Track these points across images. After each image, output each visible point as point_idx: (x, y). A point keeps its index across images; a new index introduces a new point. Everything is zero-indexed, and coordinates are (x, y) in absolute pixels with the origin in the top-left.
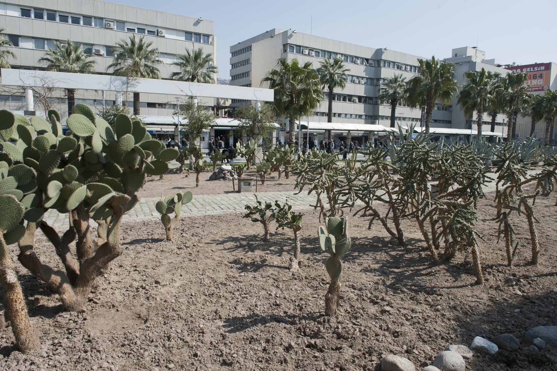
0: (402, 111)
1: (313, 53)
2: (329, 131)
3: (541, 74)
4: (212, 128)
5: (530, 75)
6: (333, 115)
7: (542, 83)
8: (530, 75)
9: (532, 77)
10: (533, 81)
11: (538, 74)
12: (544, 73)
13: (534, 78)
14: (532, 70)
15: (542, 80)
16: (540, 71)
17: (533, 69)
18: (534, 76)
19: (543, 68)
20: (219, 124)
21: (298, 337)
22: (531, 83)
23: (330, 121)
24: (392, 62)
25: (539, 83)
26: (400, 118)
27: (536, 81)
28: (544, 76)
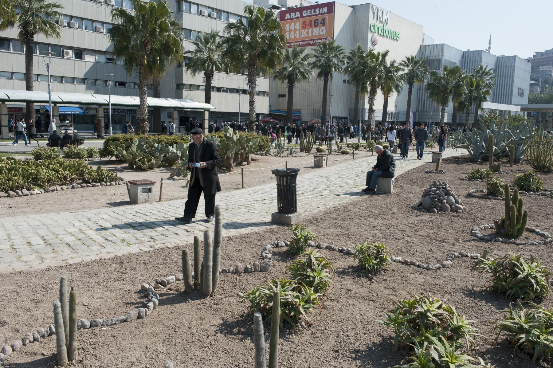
0: (220, 79)
1: (215, 15)
2: (29, 103)
3: (323, 19)
4: (55, 105)
5: (311, 21)
6: (34, 78)
7: (324, 32)
8: (311, 21)
9: (313, 23)
10: (314, 29)
11: (320, 18)
12: (327, 17)
13: (315, 26)
14: (313, 13)
15: (324, 28)
16: (322, 14)
17: (315, 12)
18: (315, 23)
19: (325, 10)
20: (64, 100)
21: (452, 221)
22: (312, 32)
23: (29, 87)
24: (224, 12)
25: (321, 33)
26: (218, 89)
27: (318, 29)
28: (327, 22)
